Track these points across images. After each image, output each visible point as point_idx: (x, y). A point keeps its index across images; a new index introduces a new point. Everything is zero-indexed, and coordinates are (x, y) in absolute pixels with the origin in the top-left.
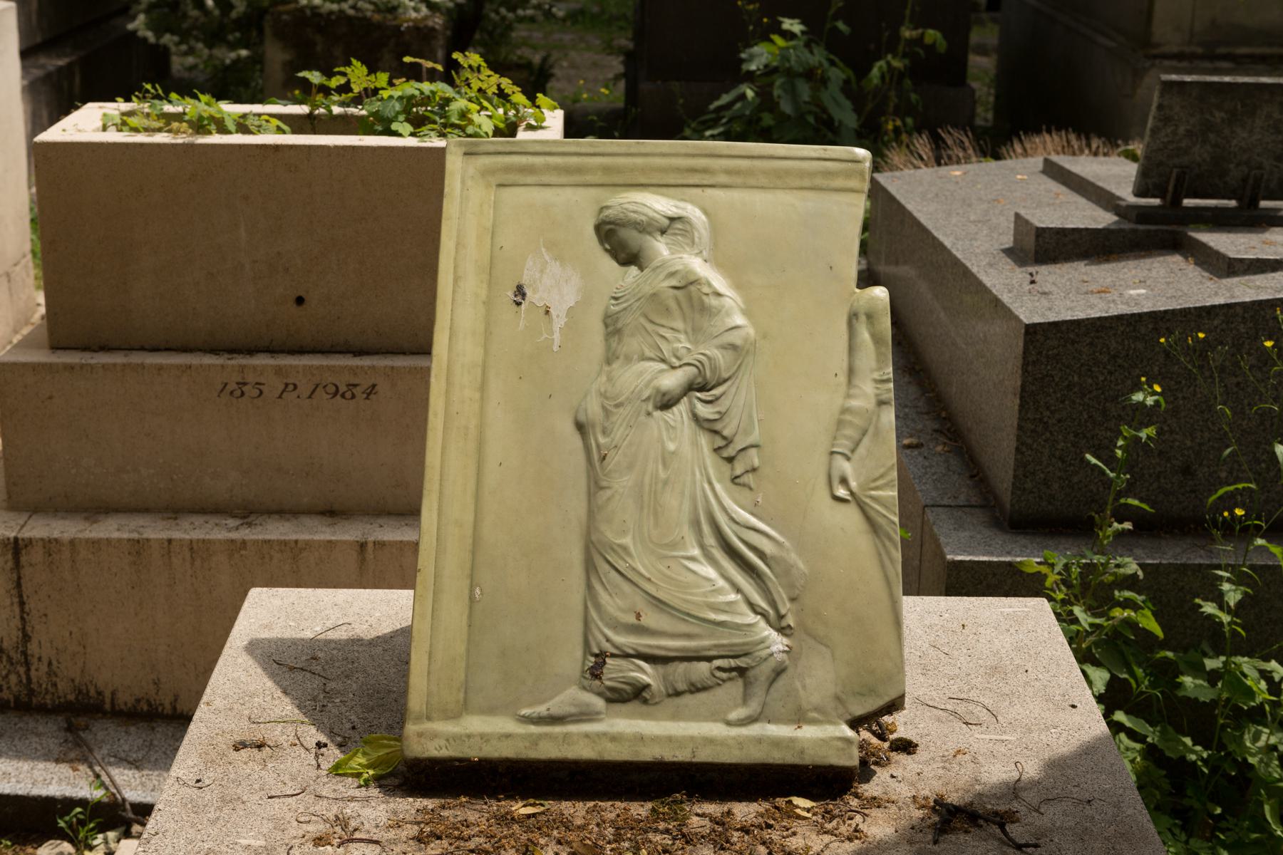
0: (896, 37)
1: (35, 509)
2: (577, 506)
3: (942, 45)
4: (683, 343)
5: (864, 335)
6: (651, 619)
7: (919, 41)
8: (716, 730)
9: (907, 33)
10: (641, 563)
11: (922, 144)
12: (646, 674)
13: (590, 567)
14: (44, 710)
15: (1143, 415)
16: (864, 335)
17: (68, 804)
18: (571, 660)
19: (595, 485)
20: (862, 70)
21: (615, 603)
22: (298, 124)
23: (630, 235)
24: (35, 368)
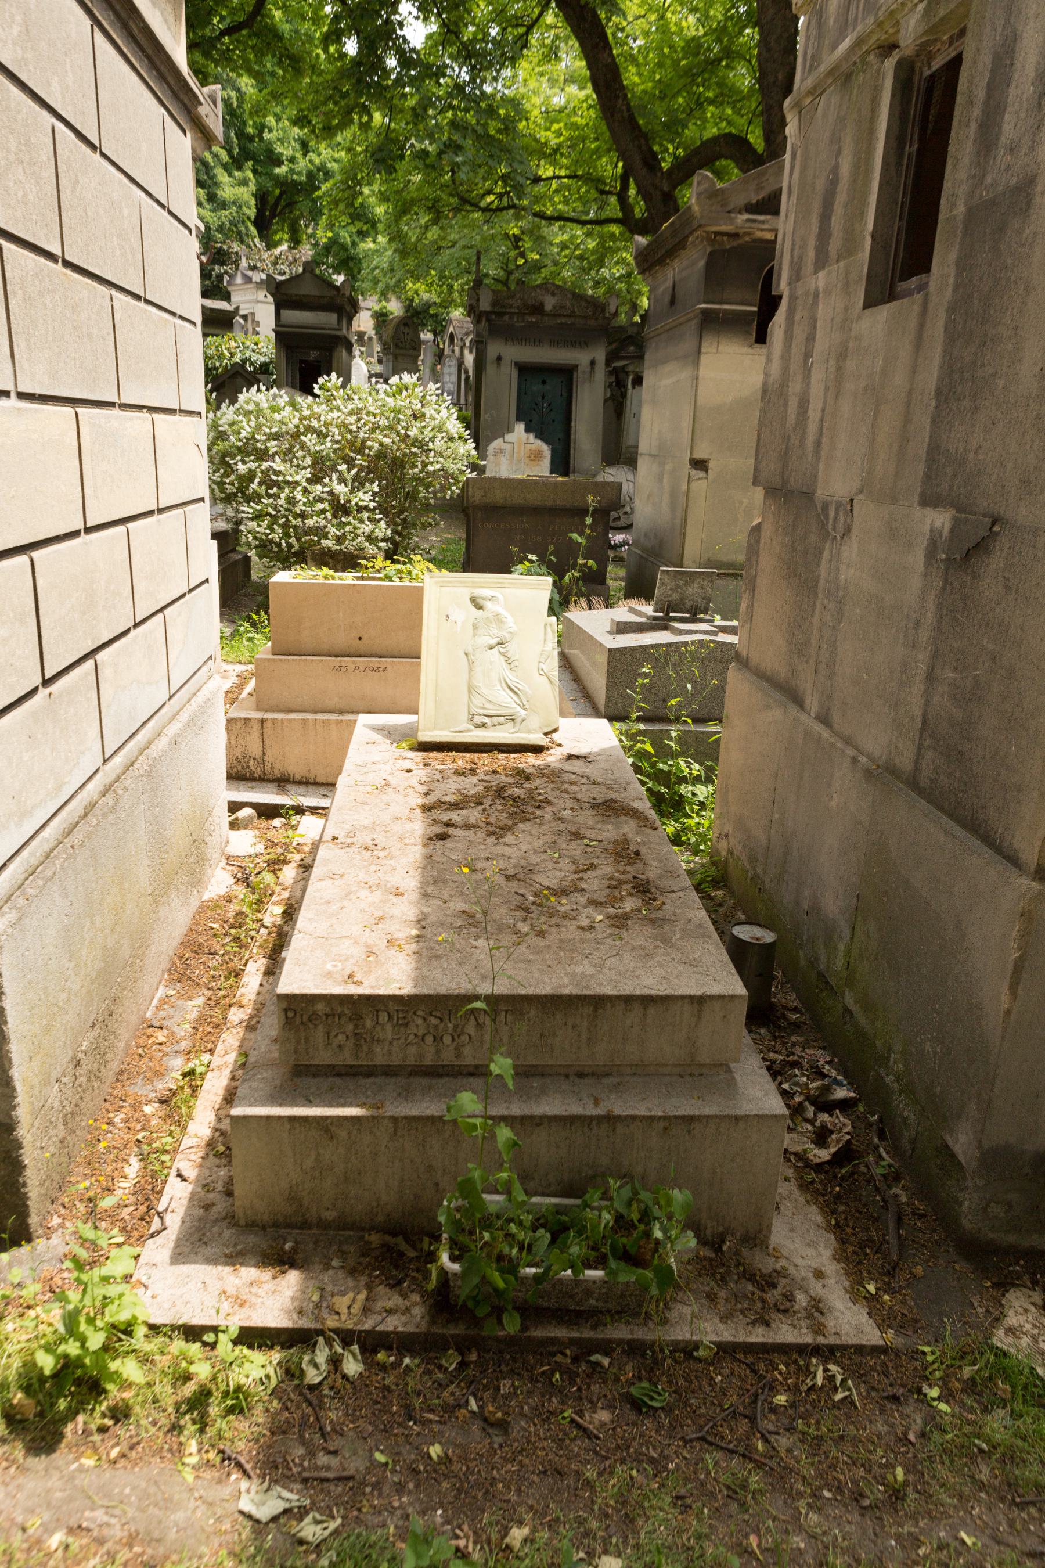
0: (575, 564)
1: (266, 711)
2: (466, 676)
3: (595, 567)
4: (496, 631)
5: (549, 630)
6: (487, 705)
7: (585, 565)
8: (506, 735)
9: (580, 561)
10: (484, 690)
11: (583, 602)
12: (486, 720)
13: (469, 691)
14: (269, 781)
15: (646, 675)
16: (549, 630)
17: (283, 806)
18: (465, 716)
19: (471, 670)
20: (561, 577)
21: (477, 701)
22: (358, 578)
23: (481, 602)
24: (268, 660)
